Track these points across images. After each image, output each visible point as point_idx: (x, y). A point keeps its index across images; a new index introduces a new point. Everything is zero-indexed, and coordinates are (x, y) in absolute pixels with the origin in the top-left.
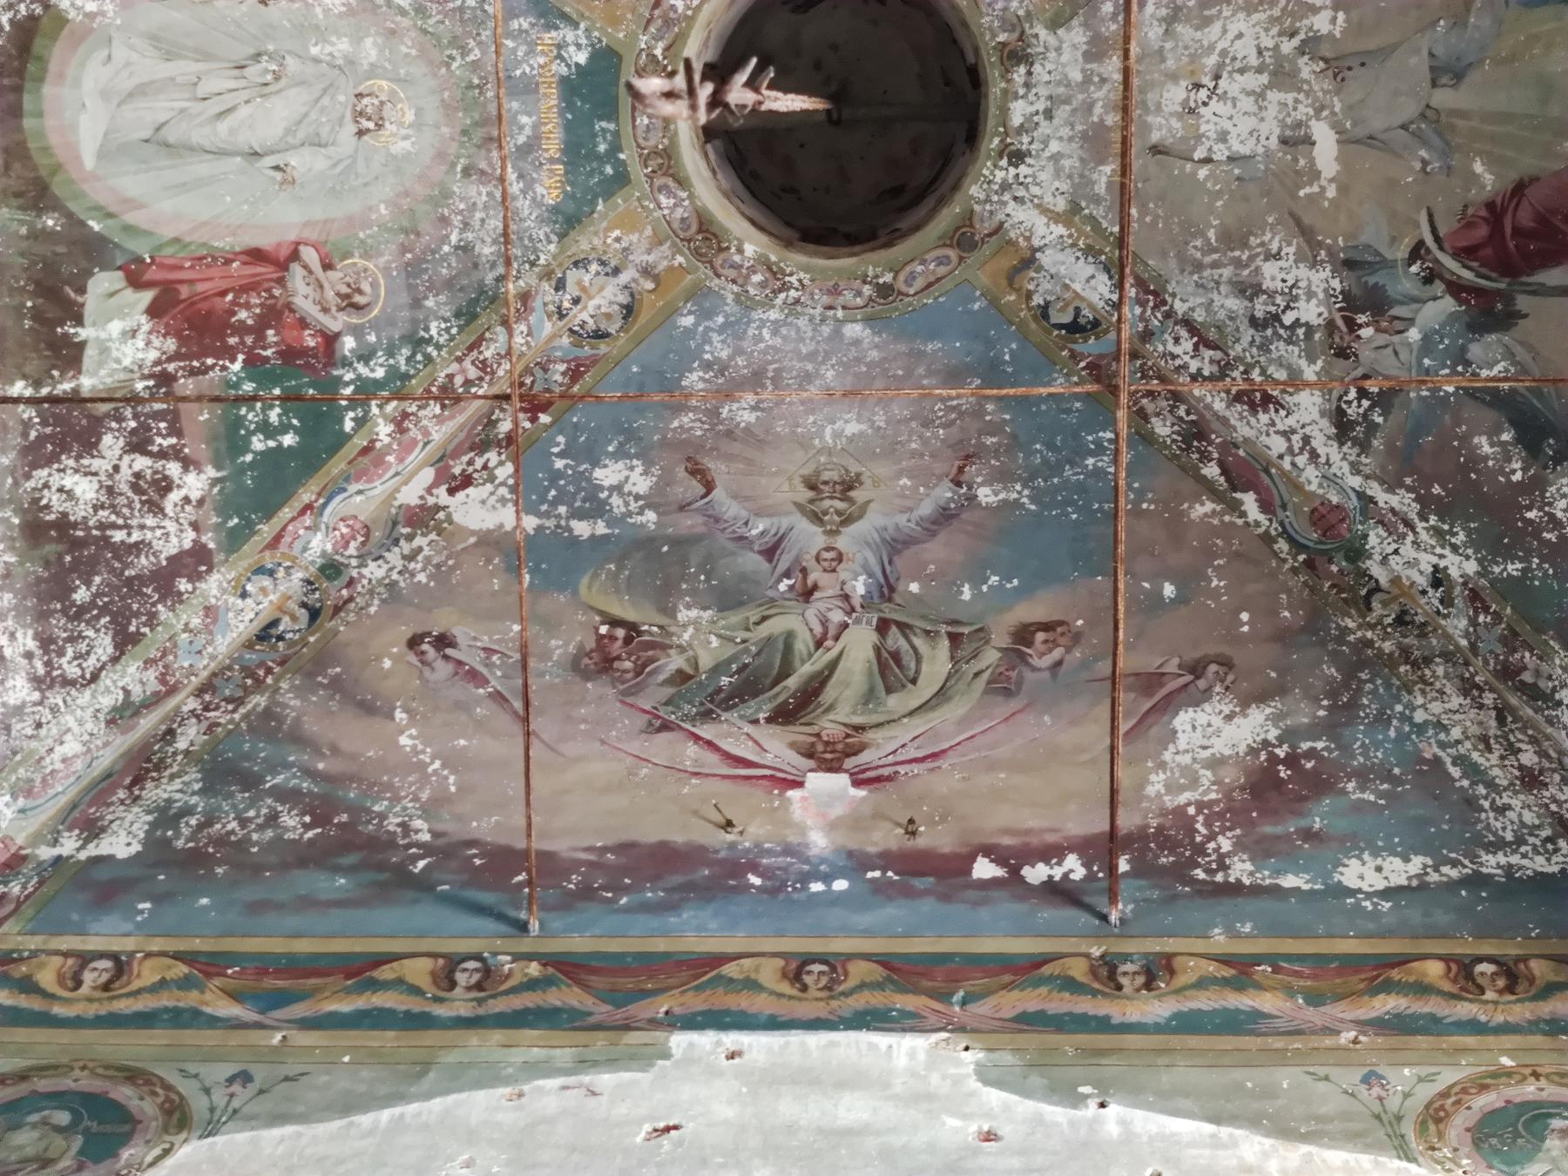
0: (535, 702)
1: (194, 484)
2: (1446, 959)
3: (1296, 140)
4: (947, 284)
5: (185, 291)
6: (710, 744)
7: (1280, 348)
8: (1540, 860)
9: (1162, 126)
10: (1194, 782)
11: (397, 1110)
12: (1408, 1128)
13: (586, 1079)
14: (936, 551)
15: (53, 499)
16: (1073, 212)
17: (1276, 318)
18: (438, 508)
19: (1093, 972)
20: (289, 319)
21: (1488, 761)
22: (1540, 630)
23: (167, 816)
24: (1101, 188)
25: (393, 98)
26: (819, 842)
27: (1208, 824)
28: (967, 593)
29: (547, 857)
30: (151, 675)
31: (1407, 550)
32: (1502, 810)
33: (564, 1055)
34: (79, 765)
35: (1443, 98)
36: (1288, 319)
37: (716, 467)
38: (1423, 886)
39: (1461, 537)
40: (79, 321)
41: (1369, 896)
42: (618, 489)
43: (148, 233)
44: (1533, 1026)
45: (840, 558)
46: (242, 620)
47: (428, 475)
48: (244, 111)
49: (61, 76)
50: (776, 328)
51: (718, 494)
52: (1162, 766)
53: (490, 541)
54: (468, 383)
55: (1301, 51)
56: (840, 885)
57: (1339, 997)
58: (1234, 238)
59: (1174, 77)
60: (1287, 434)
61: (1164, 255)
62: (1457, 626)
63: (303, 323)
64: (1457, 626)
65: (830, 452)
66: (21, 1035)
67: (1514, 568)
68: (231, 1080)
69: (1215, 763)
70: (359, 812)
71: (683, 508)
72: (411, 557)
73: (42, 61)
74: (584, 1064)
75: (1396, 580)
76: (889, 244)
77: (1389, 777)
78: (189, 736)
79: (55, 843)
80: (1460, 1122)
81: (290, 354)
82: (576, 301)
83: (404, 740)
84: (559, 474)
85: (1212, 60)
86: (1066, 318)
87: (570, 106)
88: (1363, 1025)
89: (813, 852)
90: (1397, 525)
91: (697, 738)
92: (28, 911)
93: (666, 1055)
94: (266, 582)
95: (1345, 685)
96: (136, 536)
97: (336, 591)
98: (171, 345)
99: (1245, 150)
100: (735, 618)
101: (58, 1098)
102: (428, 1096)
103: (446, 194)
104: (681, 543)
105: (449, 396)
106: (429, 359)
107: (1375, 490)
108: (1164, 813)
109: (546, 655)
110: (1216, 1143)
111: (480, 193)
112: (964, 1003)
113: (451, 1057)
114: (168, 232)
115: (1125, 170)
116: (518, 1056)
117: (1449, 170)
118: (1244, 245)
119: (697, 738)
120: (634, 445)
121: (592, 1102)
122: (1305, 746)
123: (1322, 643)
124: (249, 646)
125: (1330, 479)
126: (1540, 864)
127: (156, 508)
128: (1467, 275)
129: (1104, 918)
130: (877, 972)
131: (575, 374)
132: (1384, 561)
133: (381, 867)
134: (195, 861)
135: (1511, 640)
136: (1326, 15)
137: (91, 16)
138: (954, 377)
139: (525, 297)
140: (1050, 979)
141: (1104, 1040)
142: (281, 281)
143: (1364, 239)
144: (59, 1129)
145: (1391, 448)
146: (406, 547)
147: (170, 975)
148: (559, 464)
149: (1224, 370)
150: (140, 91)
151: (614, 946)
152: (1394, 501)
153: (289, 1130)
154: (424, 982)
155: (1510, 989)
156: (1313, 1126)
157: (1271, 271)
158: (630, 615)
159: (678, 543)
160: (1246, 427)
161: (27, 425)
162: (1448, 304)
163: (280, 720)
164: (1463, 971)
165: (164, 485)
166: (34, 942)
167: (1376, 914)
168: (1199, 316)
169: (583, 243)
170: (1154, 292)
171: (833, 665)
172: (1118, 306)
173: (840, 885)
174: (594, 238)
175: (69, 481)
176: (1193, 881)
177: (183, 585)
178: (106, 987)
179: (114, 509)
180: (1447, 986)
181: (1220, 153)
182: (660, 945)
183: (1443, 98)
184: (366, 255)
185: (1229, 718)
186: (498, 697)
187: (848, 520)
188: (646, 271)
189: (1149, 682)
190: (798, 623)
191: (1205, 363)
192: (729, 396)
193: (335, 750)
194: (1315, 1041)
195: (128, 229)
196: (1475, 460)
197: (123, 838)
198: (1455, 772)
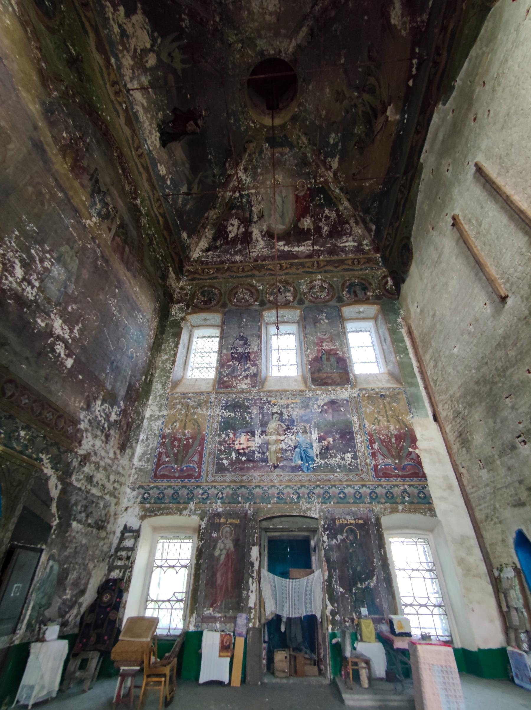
1: (327, 211)
23: (371, 220)
26: (398, 117)
42: (334, 140)
46: (346, 203)
47: (329, 172)
50: (309, 105)
53: (340, 163)
56: (406, 116)
59: (264, 19)
63: (306, 194)
93: (422, 164)
120: (327, 136)
165: (326, 216)
168: (311, 5)
171: (369, 103)
173: (406, 116)
188: (300, 130)
192: (321, 116)
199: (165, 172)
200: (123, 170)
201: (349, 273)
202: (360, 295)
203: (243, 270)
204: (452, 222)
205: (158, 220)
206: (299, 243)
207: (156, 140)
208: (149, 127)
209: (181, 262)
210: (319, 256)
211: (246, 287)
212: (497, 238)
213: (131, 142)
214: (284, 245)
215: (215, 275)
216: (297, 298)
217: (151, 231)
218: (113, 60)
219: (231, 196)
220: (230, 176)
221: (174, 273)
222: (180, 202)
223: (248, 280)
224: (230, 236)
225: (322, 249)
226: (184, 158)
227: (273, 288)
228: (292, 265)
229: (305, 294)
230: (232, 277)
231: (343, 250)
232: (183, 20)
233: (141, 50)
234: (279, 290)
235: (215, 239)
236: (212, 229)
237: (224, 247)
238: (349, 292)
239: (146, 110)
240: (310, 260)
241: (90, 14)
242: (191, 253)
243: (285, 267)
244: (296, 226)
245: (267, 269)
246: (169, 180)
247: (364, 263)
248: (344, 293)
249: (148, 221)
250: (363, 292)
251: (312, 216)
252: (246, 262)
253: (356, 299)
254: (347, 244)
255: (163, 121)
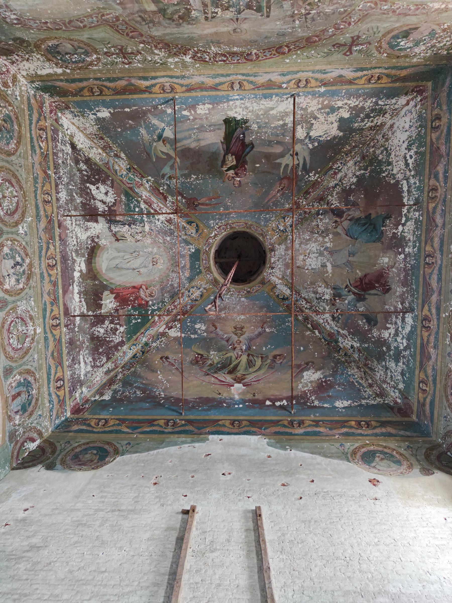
0: (184, 370)
1: (122, 329)
2: (355, 421)
3: (324, 266)
4: (260, 291)
5: (121, 294)
6: (216, 378)
7: (322, 303)
8: (373, 401)
9: (299, 263)
10: (307, 386)
11: (157, 451)
12: (349, 456)
13: (193, 444)
14: (258, 341)
15: (96, 333)
16: (283, 278)
17: (321, 298)
18: (166, 333)
19: (289, 423)
20: (140, 299)
21: (362, 382)
22: (372, 357)
23: (115, 392)
24: (288, 274)
25: (159, 259)
26: (237, 397)
27: (310, 394)
28: (264, 349)
29: (186, 400)
30: (113, 365)
31: (346, 341)
32: (365, 391)
33: (189, 440)
34: (99, 382)
35: (351, 259)
36: (323, 298)
37: (218, 325)
38: (351, 406)
39: (356, 339)
40: (102, 300)
41: (341, 408)
42: (199, 329)
43: (114, 284)
44: (373, 435)
45: (240, 342)
46: (130, 354)
47: (164, 326)
48: (132, 262)
49: (99, 256)
50: (228, 299)
51: (218, 330)
52: (301, 382)
53: (176, 339)
54: (172, 309)
55: (324, 250)
56: (241, 406)
57: (335, 429)
58: (313, 283)
59: (301, 254)
60: (323, 319)
61: (300, 286)
62: (356, 356)
63: (142, 299)
64: (356, 356)
65: (238, 322)
66: (88, 435)
67: (366, 345)
68: (127, 444)
69: (311, 382)
70: (151, 391)
71: (211, 332)
72: (161, 342)
73: (96, 254)
74: (193, 441)
75: (344, 347)
76: (249, 283)
77: (344, 385)
78: (120, 376)
79: (95, 397)
80: (359, 454)
81: (140, 305)
82: (192, 294)
83: (159, 377)
84: (189, 326)
85: (308, 251)
86: (282, 297)
87: (191, 259)
88: (340, 434)
89: (236, 399)
90: (344, 336)
91: (214, 377)
92: (89, 410)
94: (135, 347)
95: (335, 367)
96: (111, 339)
97: (147, 348)
98: (118, 304)
99: (314, 267)
100: (221, 353)
101: (94, 448)
102: (163, 448)
103: (169, 276)
104: (211, 339)
105: (169, 312)
106: (165, 305)
107: (340, 330)
108: (302, 392)
109: (186, 361)
110: (312, 458)
111: (174, 275)
112: (264, 429)
113: (168, 440)
114: (118, 284)
115: (292, 271)
116: (180, 440)
117: (352, 272)
118: (315, 285)
119: (214, 377)
120: (202, 321)
121: (194, 449)
122: (328, 379)
123: (331, 359)
124: (131, 359)
125: (331, 328)
126: (373, 402)
127: (115, 334)
128: (356, 291)
129: (291, 413)
130: (248, 423)
131: (191, 307)
132: (342, 343)
133: (155, 402)
134: (121, 400)
135: (366, 359)
136: (329, 243)
137: (105, 245)
138: (261, 308)
139: (183, 294)
140: (281, 425)
141: (291, 437)
142: (138, 292)
143: (337, 284)
144: (95, 454)
145: (342, 322)
146: (160, 340)
147: (116, 423)
148: (189, 324)
149: (311, 307)
150: (114, 258)
151: (198, 418)
152: (344, 332)
153: (137, 454)
154: (163, 425)
155: (368, 427)
156: (331, 455)
157: (320, 290)
158: (202, 353)
159: (210, 339)
160: (316, 318)
161: (91, 319)
162: (353, 296)
163: (137, 373)
164: (359, 423)
165: (116, 329)
166: (90, 417)
167: (342, 412)
168: (307, 297)
169: (193, 284)
170: (298, 293)
171: (239, 363)
172: (292, 295)
173: (241, 406)
174: (196, 283)
175: (99, 329)
176: (307, 405)
177: (119, 348)
178: (104, 425)
179: (107, 334)
180: (356, 427)
181: (310, 268)
182: (207, 418)
183: (351, 259)
184: (154, 287)
185: (314, 373)
186: (177, 368)
187: (242, 335)
188: (205, 289)
189: (299, 366)
190: (233, 354)
191: (308, 306)
193: (147, 379)
194: (331, 438)
195: (111, 283)
196: (359, 325)
197: (107, 396)
198: (356, 384)
199: (199, 112)
200: (233, 54)
201: (45, 376)
202: (16, 405)
203: (46, 202)
204: (188, 508)
205: (145, 79)
206: (84, 293)
207: (236, 112)
208: (251, 108)
209: (63, 93)
210: (66, 326)
211: (21, 204)
212: (219, 585)
213: (251, 78)
214: (81, 271)
215: (38, 151)
216: (7, 297)
217: (139, 62)
218: (322, 89)
219: (141, 197)
220: (165, 198)
221: (48, 75)
222: (155, 121)
223: (31, 210)
224: (92, 187)
225: (76, 329)
226: (203, 143)
227: (22, 253)
228: (55, 284)
229: (14, 309)
230: (35, 179)
231: (75, 361)
232: (315, 175)
233: (313, 124)
234: (18, 263)
235: (88, 161)
236: (101, 160)
237: (78, 174)
238: (19, 384)
239: (267, 112)
240: (62, 313)
241: (363, 81)
242: (70, 116)
243: (51, 272)
244: (104, 287)
245: (48, 243)
246: (188, 114)
247: (58, 396)
248: (18, 377)
249: (156, 62)
250: (20, 408)
251: (117, 310)
252: (58, 208)
253: (10, 399)
254: (82, 364)
255: (247, 128)
